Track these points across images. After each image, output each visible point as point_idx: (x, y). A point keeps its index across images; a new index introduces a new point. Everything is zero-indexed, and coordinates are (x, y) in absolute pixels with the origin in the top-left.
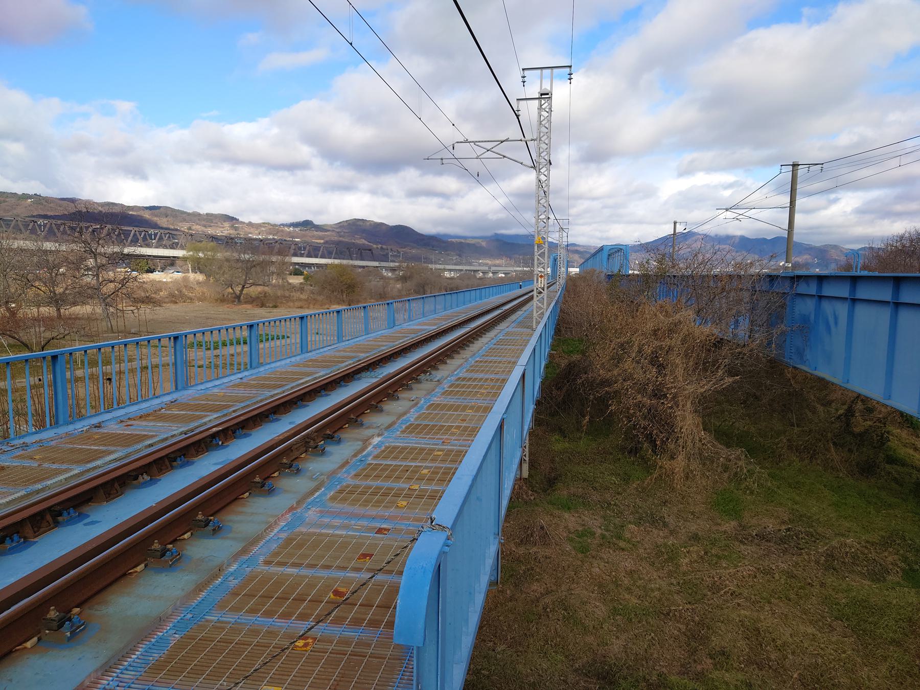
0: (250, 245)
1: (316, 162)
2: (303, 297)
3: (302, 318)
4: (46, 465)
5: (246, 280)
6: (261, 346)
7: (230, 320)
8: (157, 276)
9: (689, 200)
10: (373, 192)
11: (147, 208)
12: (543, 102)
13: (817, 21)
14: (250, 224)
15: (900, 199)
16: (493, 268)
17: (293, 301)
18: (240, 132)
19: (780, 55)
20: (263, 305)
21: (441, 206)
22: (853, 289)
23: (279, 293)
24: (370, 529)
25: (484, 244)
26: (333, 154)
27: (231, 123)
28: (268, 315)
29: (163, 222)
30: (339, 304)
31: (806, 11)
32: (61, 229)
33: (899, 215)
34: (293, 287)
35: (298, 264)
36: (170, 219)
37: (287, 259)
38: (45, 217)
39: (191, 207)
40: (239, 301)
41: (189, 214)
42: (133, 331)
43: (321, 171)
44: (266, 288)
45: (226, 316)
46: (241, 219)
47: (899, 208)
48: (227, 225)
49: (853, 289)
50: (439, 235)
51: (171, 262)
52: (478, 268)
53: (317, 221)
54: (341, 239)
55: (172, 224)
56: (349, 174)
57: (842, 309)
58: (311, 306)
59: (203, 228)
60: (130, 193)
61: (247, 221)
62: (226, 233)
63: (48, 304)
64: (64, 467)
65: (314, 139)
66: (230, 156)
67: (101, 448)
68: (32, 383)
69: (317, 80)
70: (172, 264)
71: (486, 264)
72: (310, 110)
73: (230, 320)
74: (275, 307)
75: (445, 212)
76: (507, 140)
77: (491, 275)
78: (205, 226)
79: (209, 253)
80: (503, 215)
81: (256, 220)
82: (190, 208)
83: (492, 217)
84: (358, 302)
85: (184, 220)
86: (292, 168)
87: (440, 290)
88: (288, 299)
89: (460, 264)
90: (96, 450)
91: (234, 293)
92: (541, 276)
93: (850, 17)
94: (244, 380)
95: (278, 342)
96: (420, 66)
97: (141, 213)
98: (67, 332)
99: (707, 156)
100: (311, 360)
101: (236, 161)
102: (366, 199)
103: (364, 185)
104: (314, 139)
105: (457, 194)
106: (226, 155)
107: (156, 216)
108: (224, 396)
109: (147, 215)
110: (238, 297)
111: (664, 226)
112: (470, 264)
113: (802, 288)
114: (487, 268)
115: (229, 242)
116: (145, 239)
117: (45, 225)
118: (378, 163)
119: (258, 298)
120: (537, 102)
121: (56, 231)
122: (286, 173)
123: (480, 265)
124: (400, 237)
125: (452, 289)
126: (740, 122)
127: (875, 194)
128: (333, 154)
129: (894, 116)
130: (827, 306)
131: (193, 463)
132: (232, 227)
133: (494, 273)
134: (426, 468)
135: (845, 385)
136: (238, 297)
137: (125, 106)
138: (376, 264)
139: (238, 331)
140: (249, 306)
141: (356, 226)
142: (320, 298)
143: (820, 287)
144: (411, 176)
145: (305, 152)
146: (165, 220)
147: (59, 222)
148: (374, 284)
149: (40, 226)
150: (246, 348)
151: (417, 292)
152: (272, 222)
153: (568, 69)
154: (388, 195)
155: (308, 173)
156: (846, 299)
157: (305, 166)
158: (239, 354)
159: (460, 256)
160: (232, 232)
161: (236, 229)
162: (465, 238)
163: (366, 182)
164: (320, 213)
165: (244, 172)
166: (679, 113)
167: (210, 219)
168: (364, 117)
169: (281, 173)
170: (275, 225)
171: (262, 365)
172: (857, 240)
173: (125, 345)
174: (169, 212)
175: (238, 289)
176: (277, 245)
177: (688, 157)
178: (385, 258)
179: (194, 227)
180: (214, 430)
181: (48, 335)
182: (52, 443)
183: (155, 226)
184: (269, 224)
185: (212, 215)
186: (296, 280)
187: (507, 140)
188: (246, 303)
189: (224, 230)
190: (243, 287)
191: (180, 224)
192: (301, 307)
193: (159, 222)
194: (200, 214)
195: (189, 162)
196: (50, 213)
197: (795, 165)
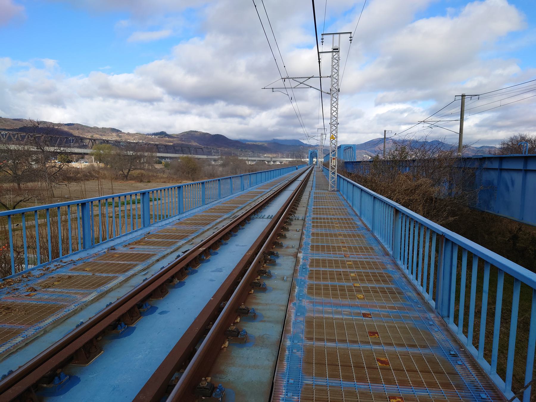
0: (129, 146)
1: (166, 97)
2: (165, 176)
3: (179, 187)
4: (98, 274)
5: (131, 166)
6: (151, 203)
7: (123, 190)
8: (74, 164)
9: (382, 119)
10: (200, 115)
11: (66, 125)
12: (334, 54)
13: (456, 14)
14: (128, 134)
15: (500, 118)
16: (274, 159)
17: (159, 178)
18: (120, 80)
19: (434, 35)
20: (141, 181)
21: (241, 123)
22: (526, 164)
23: (150, 174)
24: (358, 314)
25: (266, 145)
26: (175, 92)
27: (118, 74)
28: (146, 187)
29: (76, 133)
30: (187, 180)
31: (449, 10)
32: (16, 137)
33: (500, 128)
34: (157, 171)
35: (159, 157)
36: (80, 131)
37: (154, 154)
38: (5, 130)
39: (92, 124)
40: (127, 179)
41: (91, 128)
42: (66, 196)
43: (168, 102)
44: (143, 171)
45: (121, 188)
46: (123, 131)
47: (500, 123)
48: (114, 134)
49: (526, 164)
50: (241, 140)
51: (82, 156)
52: (264, 159)
53: (169, 132)
54: (183, 143)
55: (81, 134)
56: (186, 104)
57: (518, 178)
58: (171, 181)
59: (100, 137)
60: (56, 116)
61: (126, 132)
62: (114, 139)
63: (13, 181)
64: (111, 275)
65: (162, 83)
66: (112, 94)
67: (125, 262)
68: (12, 228)
69: (163, 48)
70: (83, 158)
71: (269, 157)
72: (160, 66)
73: (123, 190)
74: (149, 182)
75: (242, 127)
76: (312, 77)
77: (272, 163)
78: (101, 135)
79: (107, 151)
80: (276, 128)
81: (132, 131)
82: (92, 124)
83: (271, 129)
84: (198, 179)
85: (89, 132)
86: (151, 101)
87: (246, 171)
88: (157, 177)
89: (254, 157)
90: (124, 264)
91: (124, 174)
92: (334, 159)
93: (475, 10)
94: (182, 220)
95: (156, 202)
96: (224, 41)
97: (62, 128)
98: (29, 197)
99: (391, 94)
100: (212, 209)
101: (116, 96)
102: (197, 119)
103: (194, 111)
104: (162, 83)
105: (250, 116)
106: (110, 93)
107: (72, 129)
108: (177, 230)
109: (66, 129)
110: (126, 177)
111: (370, 134)
112: (259, 157)
113: (487, 165)
114: (270, 159)
115: (117, 144)
116: (66, 142)
117: (6, 135)
118: (202, 98)
119: (138, 177)
120: (331, 53)
121: (13, 138)
122: (148, 104)
123: (265, 157)
124: (217, 141)
125: (253, 171)
126: (411, 75)
127: (486, 115)
128: (175, 92)
129: (499, 71)
130: (506, 176)
131: (196, 272)
132: (118, 135)
133: (268, 162)
134: (353, 272)
135: (522, 221)
136: (126, 177)
137: (50, 62)
138: (205, 157)
139: (133, 197)
140: (133, 182)
141: (191, 135)
142: (175, 177)
143: (501, 164)
144: (221, 105)
145: (158, 91)
146: (77, 131)
147: (14, 133)
148: (207, 168)
149: (3, 135)
150: (140, 206)
151: (232, 173)
152: (142, 133)
153: (349, 35)
154: (208, 116)
155: (161, 104)
156: (520, 170)
157: (159, 100)
158: (134, 209)
159: (253, 152)
160: (118, 139)
161: (120, 137)
162: (255, 141)
163: (197, 109)
164: (170, 127)
165: (122, 103)
166: (376, 70)
167: (104, 130)
168: (191, 70)
169: (144, 104)
170: (144, 135)
171: (183, 213)
172: (477, 142)
173: (69, 206)
174: (79, 127)
175: (126, 172)
176: (146, 146)
177: (381, 94)
178: (209, 153)
179: (94, 136)
180: (201, 249)
181: (19, 199)
182: (90, 260)
183: (71, 135)
184: (140, 134)
185: (105, 128)
186: (158, 166)
187: (312, 77)
188: (131, 180)
189: (113, 137)
190: (129, 170)
191: (86, 134)
192: (165, 182)
193: (73, 133)
194: (98, 128)
195: (90, 97)
196: (7, 128)
197: (463, 96)
